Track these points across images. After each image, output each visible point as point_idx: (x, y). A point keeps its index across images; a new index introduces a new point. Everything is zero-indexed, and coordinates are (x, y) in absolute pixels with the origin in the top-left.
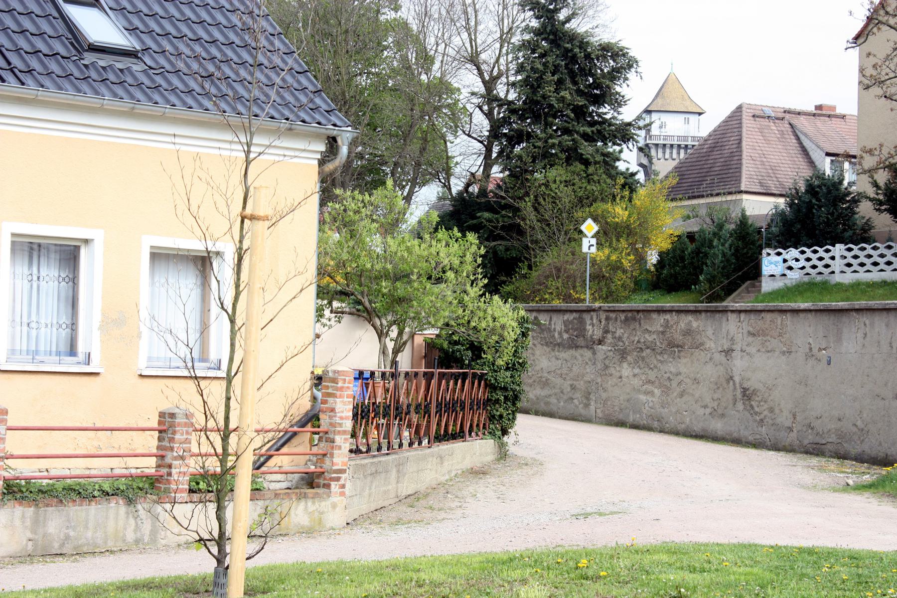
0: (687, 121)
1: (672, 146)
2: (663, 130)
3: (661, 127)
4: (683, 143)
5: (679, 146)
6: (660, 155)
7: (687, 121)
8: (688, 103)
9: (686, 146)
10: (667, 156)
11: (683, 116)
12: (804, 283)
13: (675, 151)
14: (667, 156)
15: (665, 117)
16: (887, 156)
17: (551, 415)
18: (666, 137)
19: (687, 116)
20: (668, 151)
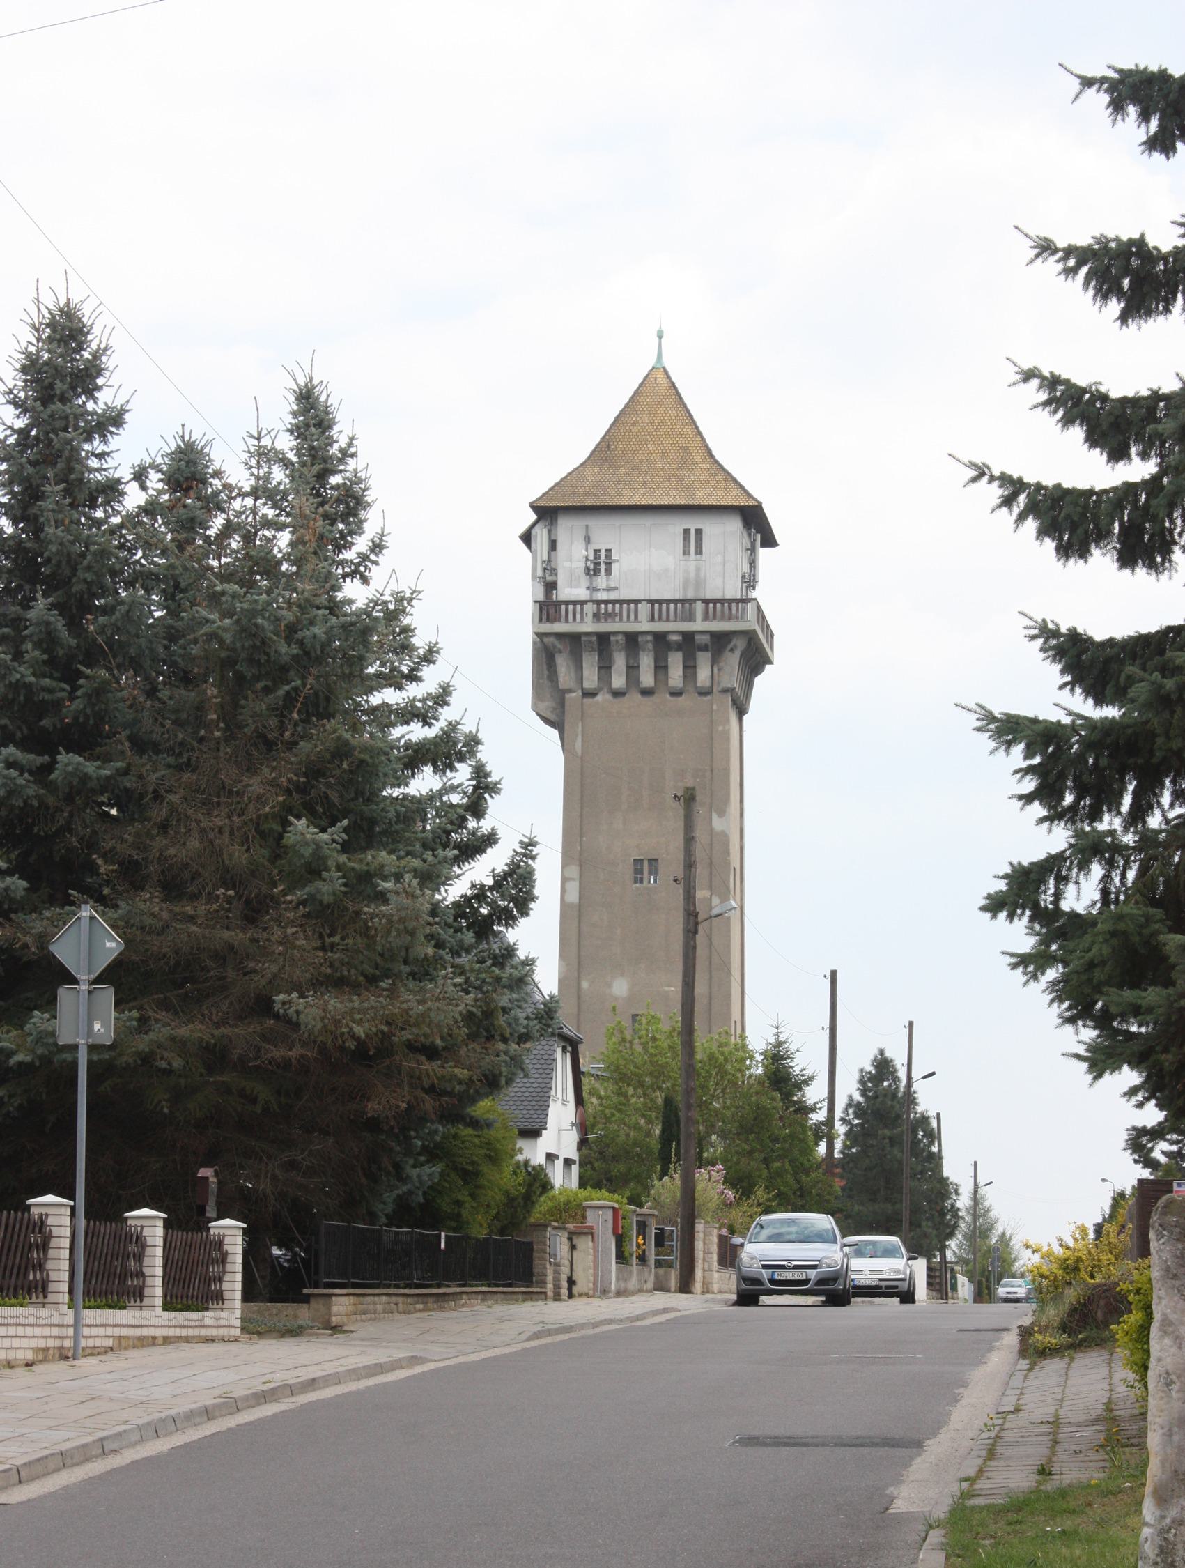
0: (693, 543)
1: (632, 640)
2: (601, 581)
3: (592, 571)
4: (674, 626)
5: (660, 639)
6: (591, 677)
7: (693, 543)
8: (700, 474)
9: (688, 637)
10: (618, 681)
11: (675, 527)
12: (893, 1485)
13: (646, 662)
14: (618, 681)
15: (607, 533)
16: (924, 1528)
17: (707, 446)
18: (606, 608)
19: (693, 523)
20: (620, 661)
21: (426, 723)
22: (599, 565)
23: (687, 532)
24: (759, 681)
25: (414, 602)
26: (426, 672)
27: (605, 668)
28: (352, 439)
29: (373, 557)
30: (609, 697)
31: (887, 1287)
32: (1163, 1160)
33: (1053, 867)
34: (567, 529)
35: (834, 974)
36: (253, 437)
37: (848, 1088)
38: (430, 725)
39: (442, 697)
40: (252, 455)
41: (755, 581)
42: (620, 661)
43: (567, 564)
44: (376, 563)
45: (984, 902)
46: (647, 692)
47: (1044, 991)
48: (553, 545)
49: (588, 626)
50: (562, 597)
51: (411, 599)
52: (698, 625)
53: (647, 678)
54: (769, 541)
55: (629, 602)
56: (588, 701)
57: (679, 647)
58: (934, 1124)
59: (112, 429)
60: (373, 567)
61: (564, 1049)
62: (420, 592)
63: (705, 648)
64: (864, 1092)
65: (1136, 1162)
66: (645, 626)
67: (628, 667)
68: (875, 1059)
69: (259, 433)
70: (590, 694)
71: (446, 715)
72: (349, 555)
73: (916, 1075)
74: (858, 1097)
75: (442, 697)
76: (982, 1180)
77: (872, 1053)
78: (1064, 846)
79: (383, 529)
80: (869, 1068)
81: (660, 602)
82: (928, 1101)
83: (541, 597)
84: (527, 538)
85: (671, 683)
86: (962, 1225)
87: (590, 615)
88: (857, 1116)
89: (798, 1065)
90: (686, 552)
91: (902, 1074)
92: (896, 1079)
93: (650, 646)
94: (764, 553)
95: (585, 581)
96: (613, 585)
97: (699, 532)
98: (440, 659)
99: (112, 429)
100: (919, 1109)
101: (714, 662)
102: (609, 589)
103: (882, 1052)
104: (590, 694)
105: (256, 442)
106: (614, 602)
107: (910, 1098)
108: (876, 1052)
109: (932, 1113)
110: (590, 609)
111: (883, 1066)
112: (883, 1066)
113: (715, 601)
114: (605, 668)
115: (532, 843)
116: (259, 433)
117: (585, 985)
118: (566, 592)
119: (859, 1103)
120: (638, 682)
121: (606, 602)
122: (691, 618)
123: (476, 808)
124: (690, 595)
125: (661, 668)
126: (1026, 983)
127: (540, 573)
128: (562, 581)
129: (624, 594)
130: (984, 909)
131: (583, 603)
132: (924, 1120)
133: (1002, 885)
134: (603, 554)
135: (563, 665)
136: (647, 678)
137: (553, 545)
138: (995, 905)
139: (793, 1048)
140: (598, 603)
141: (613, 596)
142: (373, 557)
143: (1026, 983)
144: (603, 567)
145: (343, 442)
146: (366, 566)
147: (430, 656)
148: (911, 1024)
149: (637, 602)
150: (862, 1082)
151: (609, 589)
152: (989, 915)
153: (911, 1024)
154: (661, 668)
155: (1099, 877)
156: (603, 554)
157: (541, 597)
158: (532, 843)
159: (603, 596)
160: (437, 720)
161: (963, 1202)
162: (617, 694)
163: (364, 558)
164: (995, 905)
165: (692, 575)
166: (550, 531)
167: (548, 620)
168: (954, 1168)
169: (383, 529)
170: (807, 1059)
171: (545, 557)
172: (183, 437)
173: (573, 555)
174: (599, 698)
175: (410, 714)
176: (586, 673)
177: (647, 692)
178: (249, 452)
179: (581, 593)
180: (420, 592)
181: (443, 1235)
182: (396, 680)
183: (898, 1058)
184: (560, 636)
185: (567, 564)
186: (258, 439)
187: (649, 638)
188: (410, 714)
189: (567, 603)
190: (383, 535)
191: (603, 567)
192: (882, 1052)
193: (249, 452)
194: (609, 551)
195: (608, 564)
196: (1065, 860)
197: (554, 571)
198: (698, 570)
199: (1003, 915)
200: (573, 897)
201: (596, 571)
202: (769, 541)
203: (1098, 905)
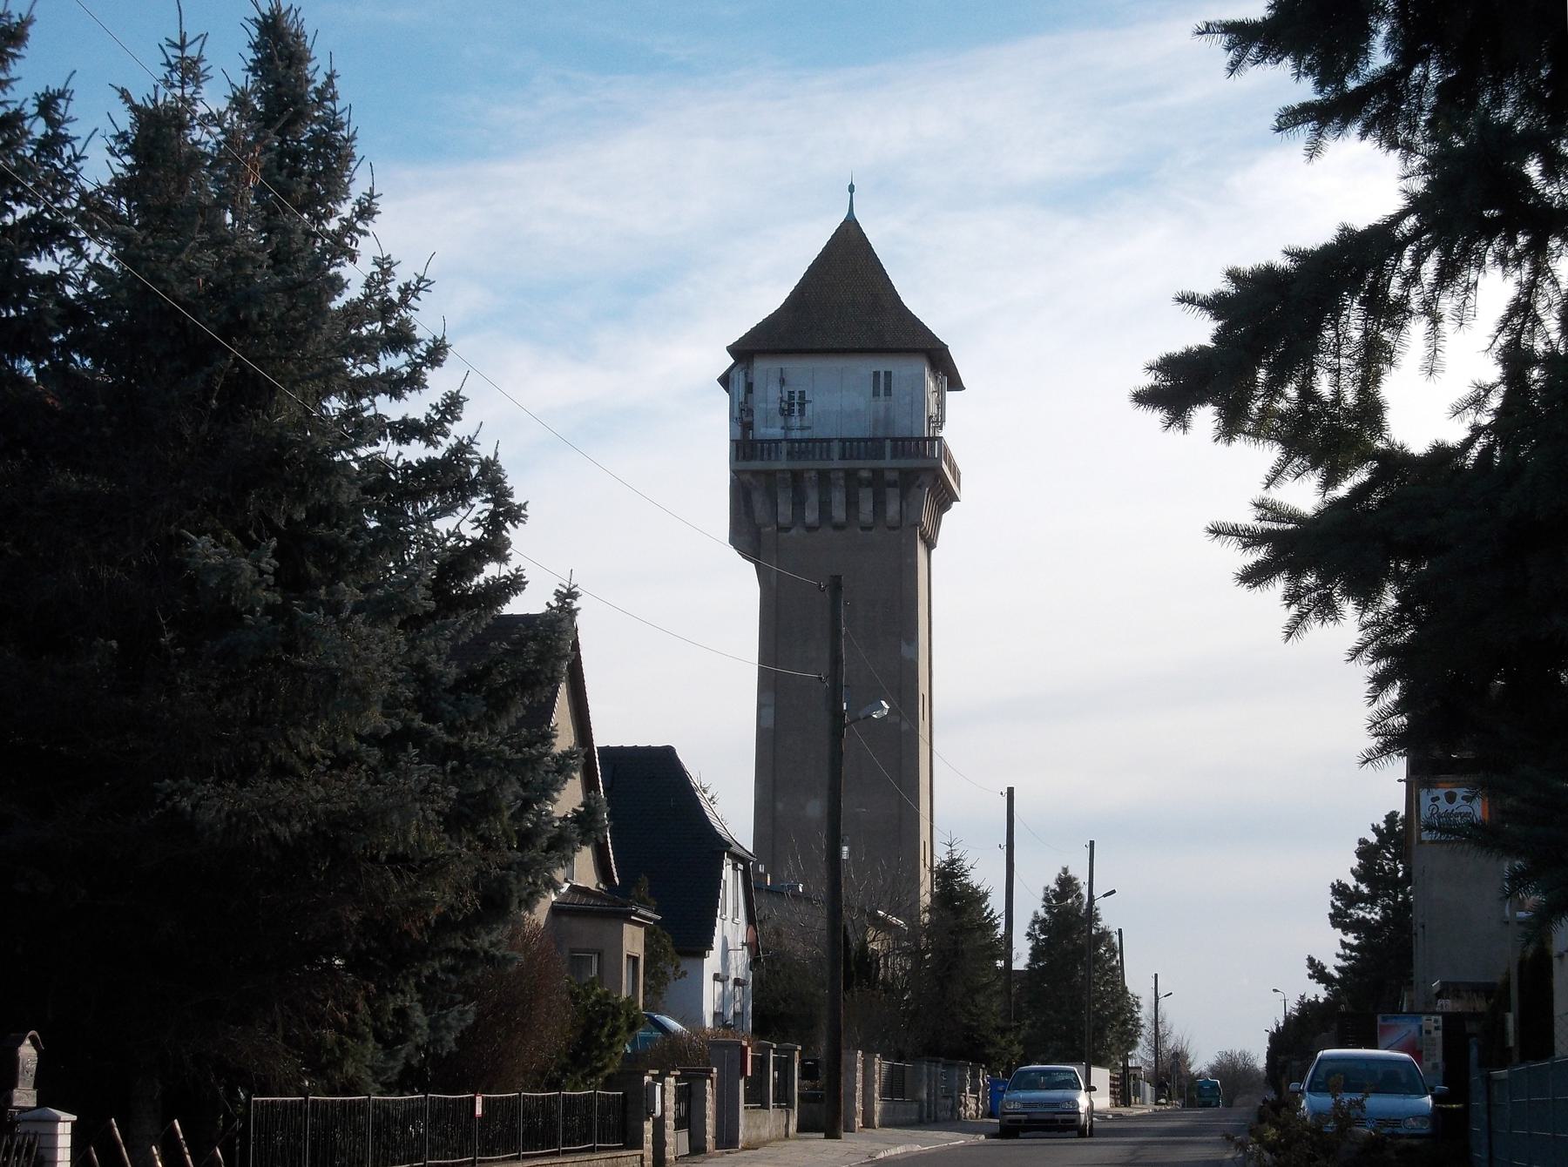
1: (824, 477)
2: (795, 421)
3: (786, 412)
6: (785, 511)
10: (811, 516)
14: (811, 516)
21: (431, 443)
22: (792, 405)
23: (876, 374)
24: (946, 516)
25: (421, 294)
26: (431, 375)
27: (799, 504)
28: (331, 77)
29: (360, 225)
30: (802, 531)
31: (1064, 1121)
32: (1336, 975)
33: (1350, 268)
34: (764, 368)
35: (1010, 791)
36: (174, 45)
37: (1030, 906)
38: (436, 444)
39: (452, 406)
40: (173, 68)
41: (943, 421)
42: (813, 498)
43: (762, 405)
44: (365, 233)
45: (1148, 380)
46: (838, 527)
47: (1356, 653)
48: (749, 388)
49: (782, 464)
50: (758, 437)
51: (418, 289)
52: (887, 462)
53: (839, 514)
54: (956, 384)
55: (822, 440)
56: (783, 535)
57: (869, 484)
58: (1116, 939)
59: (10, 50)
60: (362, 239)
61: (735, 868)
62: (430, 283)
63: (893, 484)
64: (1049, 909)
65: (1310, 977)
66: (836, 463)
67: (820, 502)
68: (1060, 878)
69: (183, 40)
70: (782, 529)
71: (457, 431)
72: (333, 225)
73: (1096, 894)
74: (1042, 913)
75: (452, 406)
76: (1161, 993)
77: (1056, 872)
78: (1397, 203)
79: (372, 190)
80: (1054, 886)
81: (851, 440)
82: (1109, 917)
83: (738, 437)
84: (725, 381)
85: (862, 517)
86: (1144, 1031)
87: (784, 452)
88: (1042, 931)
89: (975, 878)
90: (876, 394)
91: (1085, 891)
92: (1079, 896)
93: (842, 482)
94: (951, 396)
95: (780, 421)
96: (806, 424)
97: (888, 374)
98: (450, 358)
99: (10, 50)
100: (1101, 924)
101: (903, 497)
102: (802, 428)
103: (1065, 870)
104: (782, 529)
105: (178, 53)
106: (808, 440)
107: (1091, 916)
108: (1060, 871)
109: (1113, 929)
110: (784, 446)
111: (1066, 884)
112: (1066, 884)
113: (903, 439)
114: (799, 504)
115: (572, 595)
116: (183, 40)
117: (780, 806)
118: (762, 431)
119: (1044, 920)
120: (831, 517)
121: (800, 441)
122: (882, 457)
123: (493, 547)
124: (880, 434)
125: (852, 504)
126: (1293, 629)
127: (737, 414)
128: (758, 417)
129: (817, 433)
130: (1145, 398)
131: (777, 441)
132: (1105, 935)
133: (1201, 331)
134: (797, 395)
135: (758, 500)
136: (839, 514)
137: (749, 388)
138: (1179, 387)
139: (967, 865)
140: (792, 441)
141: (806, 434)
142: (360, 225)
143: (1293, 629)
144: (796, 407)
145: (320, 80)
146: (352, 237)
147: (436, 353)
148: (1092, 843)
149: (829, 441)
150: (1046, 899)
151: (802, 428)
152: (1157, 416)
153: (1092, 843)
154: (852, 504)
155: (1502, 310)
156: (797, 395)
157: (738, 437)
158: (572, 595)
159: (796, 435)
160: (446, 435)
161: (1144, 1014)
162: (810, 528)
163: (348, 227)
164: (1179, 387)
165: (882, 414)
166: (746, 375)
167: (744, 458)
168: (1136, 982)
169: (372, 190)
170: (985, 874)
171: (742, 399)
172: (155, 100)
173: (769, 396)
174: (793, 532)
175: (407, 430)
176: (780, 509)
177: (838, 527)
178: (169, 64)
179: (776, 432)
180: (430, 283)
181: (479, 1100)
182: (396, 385)
183: (1082, 879)
184: (755, 473)
185: (762, 405)
186: (182, 47)
187: (841, 474)
188: (407, 430)
189: (762, 442)
190: (372, 196)
191: (796, 407)
192: (1065, 870)
193: (169, 64)
194: (802, 393)
195: (802, 405)
196: (1399, 247)
197: (750, 412)
198: (887, 409)
199: (1205, 417)
200: (770, 723)
201: (790, 412)
202: (956, 384)
203: (1495, 401)
